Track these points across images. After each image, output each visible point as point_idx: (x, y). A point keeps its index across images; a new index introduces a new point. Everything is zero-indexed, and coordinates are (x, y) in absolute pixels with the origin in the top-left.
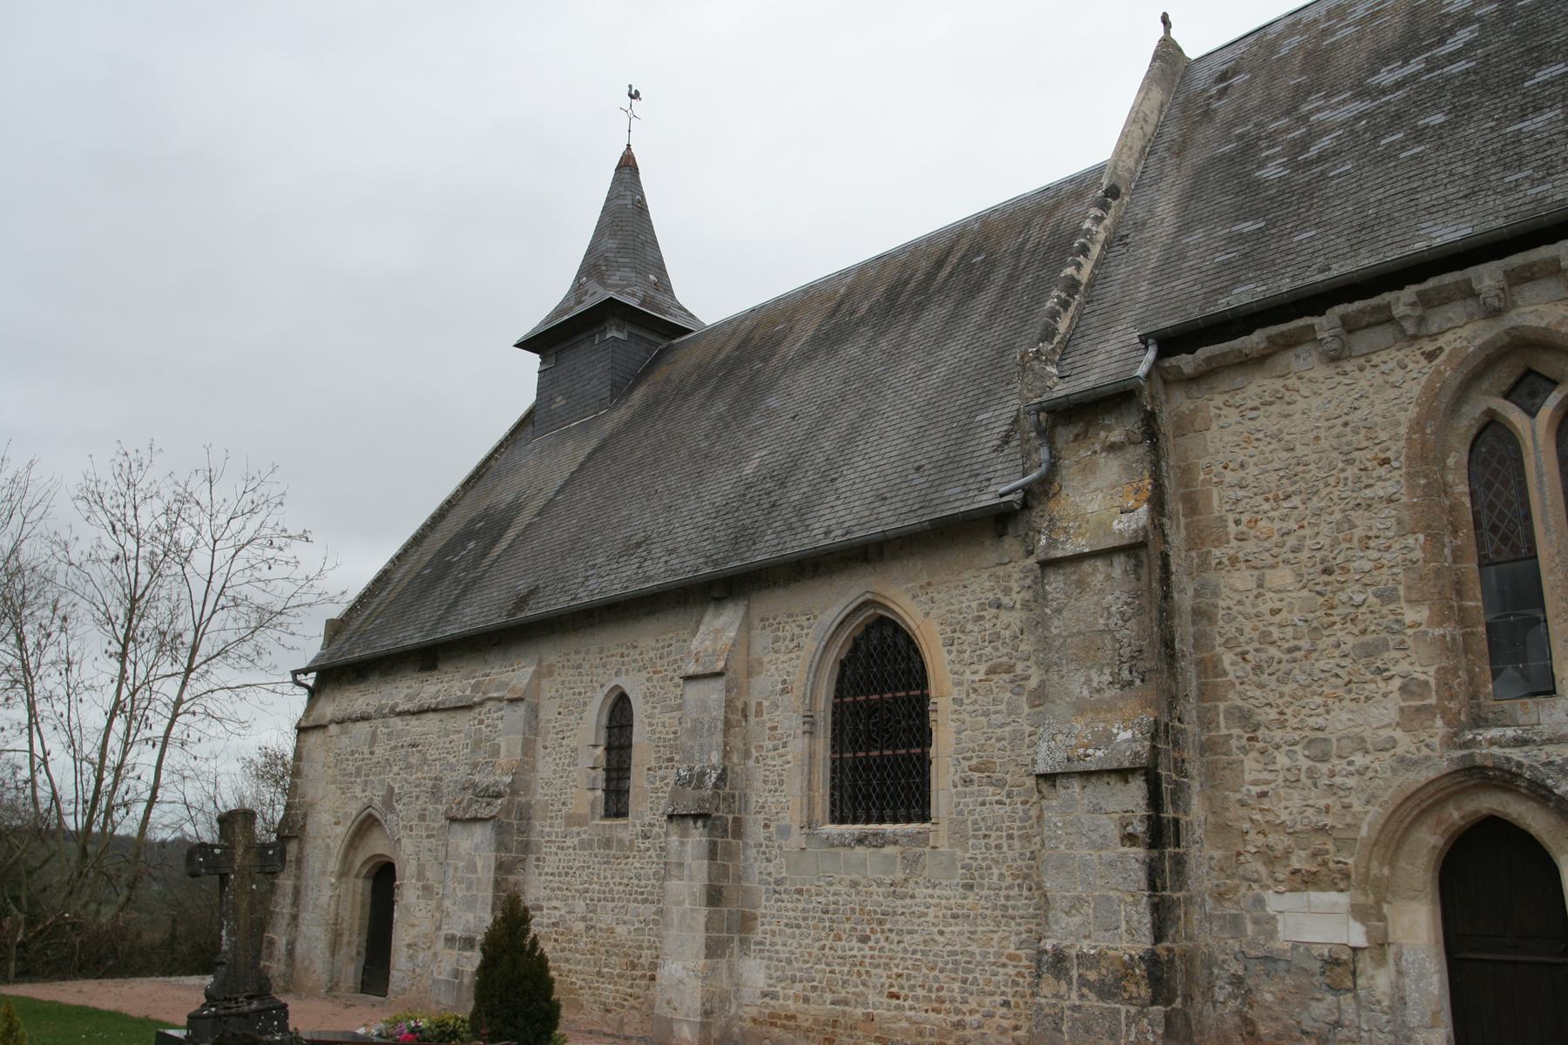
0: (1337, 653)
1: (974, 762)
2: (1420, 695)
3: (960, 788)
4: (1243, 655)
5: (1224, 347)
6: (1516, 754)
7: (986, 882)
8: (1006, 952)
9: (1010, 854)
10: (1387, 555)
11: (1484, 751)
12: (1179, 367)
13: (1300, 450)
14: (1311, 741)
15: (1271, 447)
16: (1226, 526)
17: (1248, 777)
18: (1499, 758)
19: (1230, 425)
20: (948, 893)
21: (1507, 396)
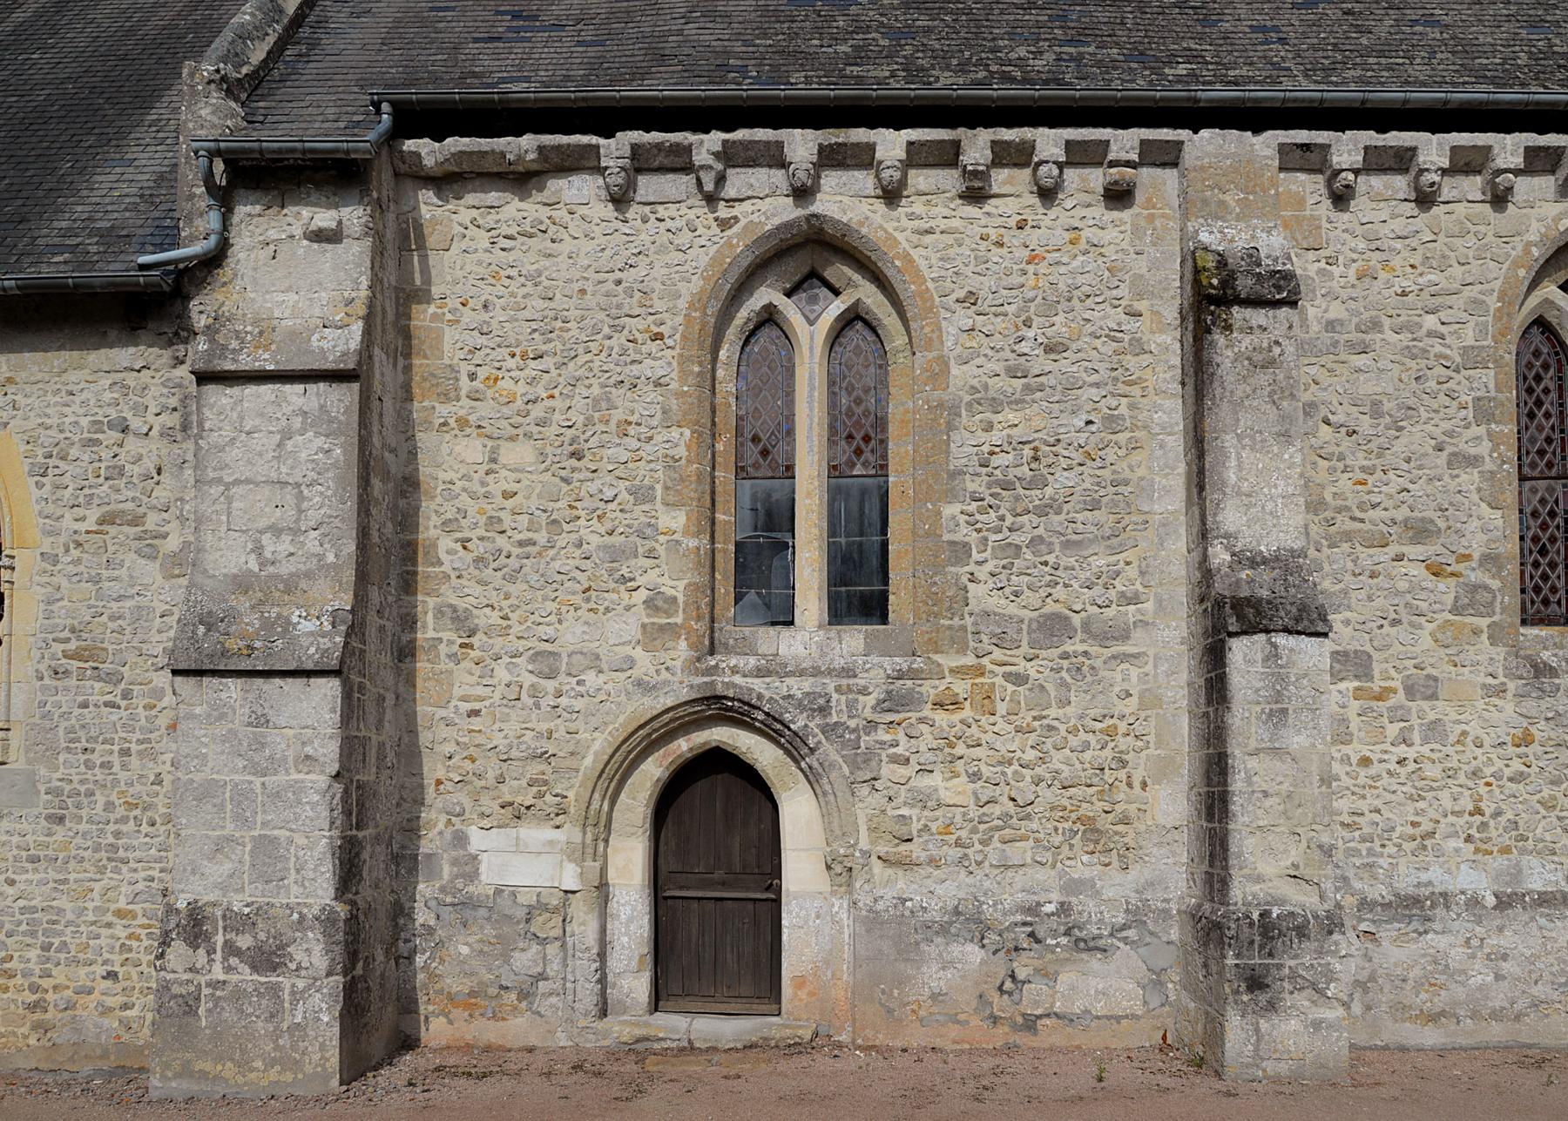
0: (578, 553)
1: (72, 645)
2: (666, 612)
3: (47, 681)
4: (464, 543)
5: (484, 144)
6: (758, 684)
7: (84, 813)
8: (113, 907)
9: (123, 776)
10: (648, 447)
11: (726, 680)
12: (418, 155)
13: (559, 302)
14: (537, 654)
15: (524, 290)
16: (457, 380)
17: (457, 692)
18: (741, 688)
19: (476, 250)
20: (25, 826)
21: (789, 294)
